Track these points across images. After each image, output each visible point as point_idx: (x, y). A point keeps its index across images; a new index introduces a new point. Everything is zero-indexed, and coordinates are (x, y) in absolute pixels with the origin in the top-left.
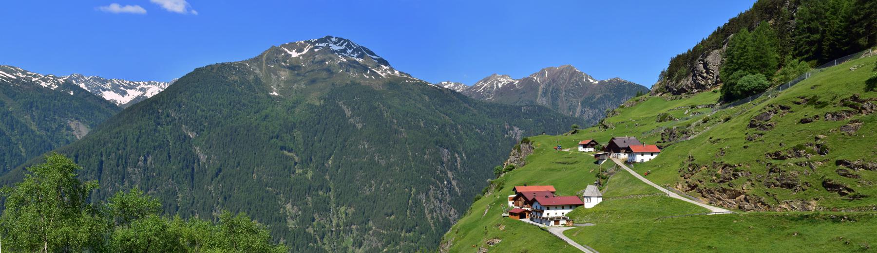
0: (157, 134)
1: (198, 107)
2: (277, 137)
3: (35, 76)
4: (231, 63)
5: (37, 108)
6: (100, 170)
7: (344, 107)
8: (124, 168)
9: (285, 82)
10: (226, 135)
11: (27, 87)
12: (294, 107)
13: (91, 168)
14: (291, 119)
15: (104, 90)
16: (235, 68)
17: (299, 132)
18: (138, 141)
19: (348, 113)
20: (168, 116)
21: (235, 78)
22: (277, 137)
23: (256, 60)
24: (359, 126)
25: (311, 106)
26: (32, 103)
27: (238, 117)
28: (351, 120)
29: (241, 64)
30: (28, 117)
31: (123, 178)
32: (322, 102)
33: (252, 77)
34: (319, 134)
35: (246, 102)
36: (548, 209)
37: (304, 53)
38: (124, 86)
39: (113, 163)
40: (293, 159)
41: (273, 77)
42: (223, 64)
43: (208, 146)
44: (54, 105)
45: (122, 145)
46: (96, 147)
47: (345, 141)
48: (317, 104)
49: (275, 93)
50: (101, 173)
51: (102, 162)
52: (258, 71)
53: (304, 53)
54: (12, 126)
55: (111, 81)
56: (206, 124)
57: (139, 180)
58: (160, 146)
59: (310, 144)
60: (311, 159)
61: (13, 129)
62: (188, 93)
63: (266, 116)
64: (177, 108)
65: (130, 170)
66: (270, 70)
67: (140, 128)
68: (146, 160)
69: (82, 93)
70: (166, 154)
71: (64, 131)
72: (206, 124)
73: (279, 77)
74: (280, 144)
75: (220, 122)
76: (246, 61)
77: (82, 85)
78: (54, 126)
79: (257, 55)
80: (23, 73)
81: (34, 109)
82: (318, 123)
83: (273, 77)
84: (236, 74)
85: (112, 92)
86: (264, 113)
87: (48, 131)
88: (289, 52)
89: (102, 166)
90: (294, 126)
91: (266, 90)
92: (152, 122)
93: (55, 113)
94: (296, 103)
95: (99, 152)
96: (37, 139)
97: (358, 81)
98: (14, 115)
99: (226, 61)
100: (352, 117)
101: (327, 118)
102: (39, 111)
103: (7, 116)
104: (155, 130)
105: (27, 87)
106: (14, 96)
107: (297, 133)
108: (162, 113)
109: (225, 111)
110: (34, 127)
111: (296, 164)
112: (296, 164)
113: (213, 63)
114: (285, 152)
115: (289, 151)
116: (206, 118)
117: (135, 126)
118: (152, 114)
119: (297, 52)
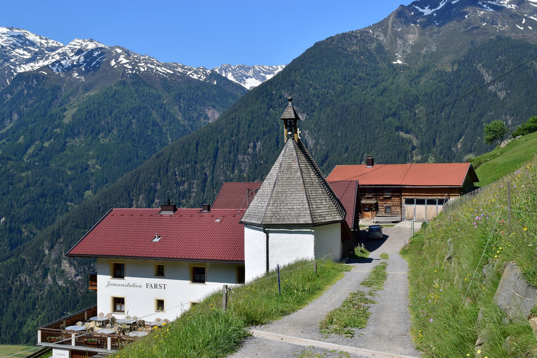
0: (268, 118)
1: (311, 85)
2: (394, 115)
3: (190, 70)
4: (353, 32)
5: (184, 99)
6: (215, 157)
7: (483, 71)
8: (236, 156)
9: (413, 47)
10: (336, 115)
11: (180, 80)
12: (419, 76)
13: (208, 156)
14: (414, 91)
15: (247, 78)
16: (356, 37)
17: (422, 108)
18: (249, 126)
19: (488, 78)
20: (281, 97)
21: (355, 48)
22: (394, 115)
23: (382, 25)
24: (502, 95)
25: (441, 74)
26: (180, 94)
27: (352, 93)
28: (491, 87)
29: (363, 32)
30: (176, 108)
31: (234, 166)
32: (455, 67)
33: (374, 45)
34: (447, 109)
35: (363, 75)
36: (118, 272)
37: (439, 8)
38: (264, 72)
39: (226, 150)
40: (410, 142)
41: (399, 42)
42: (343, 34)
43: (316, 129)
44: (197, 95)
45: (235, 131)
46: (214, 134)
47: (481, 116)
48: (449, 69)
49: (399, 62)
50: (216, 161)
51: (217, 149)
52: (381, 38)
53: (439, 8)
54: (164, 117)
55: (253, 67)
56: (317, 104)
57: (247, 169)
58: (269, 131)
59: (435, 122)
60: (434, 143)
61: (165, 120)
62: (303, 71)
63: (385, 90)
64: (290, 88)
65: (240, 157)
66: (396, 35)
67: (252, 112)
68: (255, 146)
69: (223, 82)
70: (274, 140)
71: (202, 119)
72: (317, 104)
73: (406, 41)
74: (396, 122)
75: (331, 101)
76: (370, 27)
77: (230, 77)
78: (195, 115)
79: (382, 19)
80: (182, 67)
81: (181, 100)
82: (447, 95)
83: (399, 42)
84: (356, 45)
85: (253, 79)
86: (381, 87)
87: (190, 120)
88: (421, 10)
89: (217, 153)
90: (417, 100)
91: (388, 58)
92: (265, 105)
93: (196, 102)
94: (422, 71)
95: (216, 140)
96: (181, 128)
97: (507, 35)
98: (167, 107)
99: (346, 30)
100: (493, 82)
101: (459, 87)
102: (185, 102)
103: (161, 108)
104: (267, 114)
105: (180, 80)
106: (169, 89)
107: (420, 110)
108: (276, 94)
109: (339, 87)
110: (180, 118)
111: (414, 148)
112: (414, 148)
113: (333, 35)
114: (402, 134)
115: (407, 133)
116: (318, 97)
117: (249, 109)
118: (266, 97)
119: (431, 8)
